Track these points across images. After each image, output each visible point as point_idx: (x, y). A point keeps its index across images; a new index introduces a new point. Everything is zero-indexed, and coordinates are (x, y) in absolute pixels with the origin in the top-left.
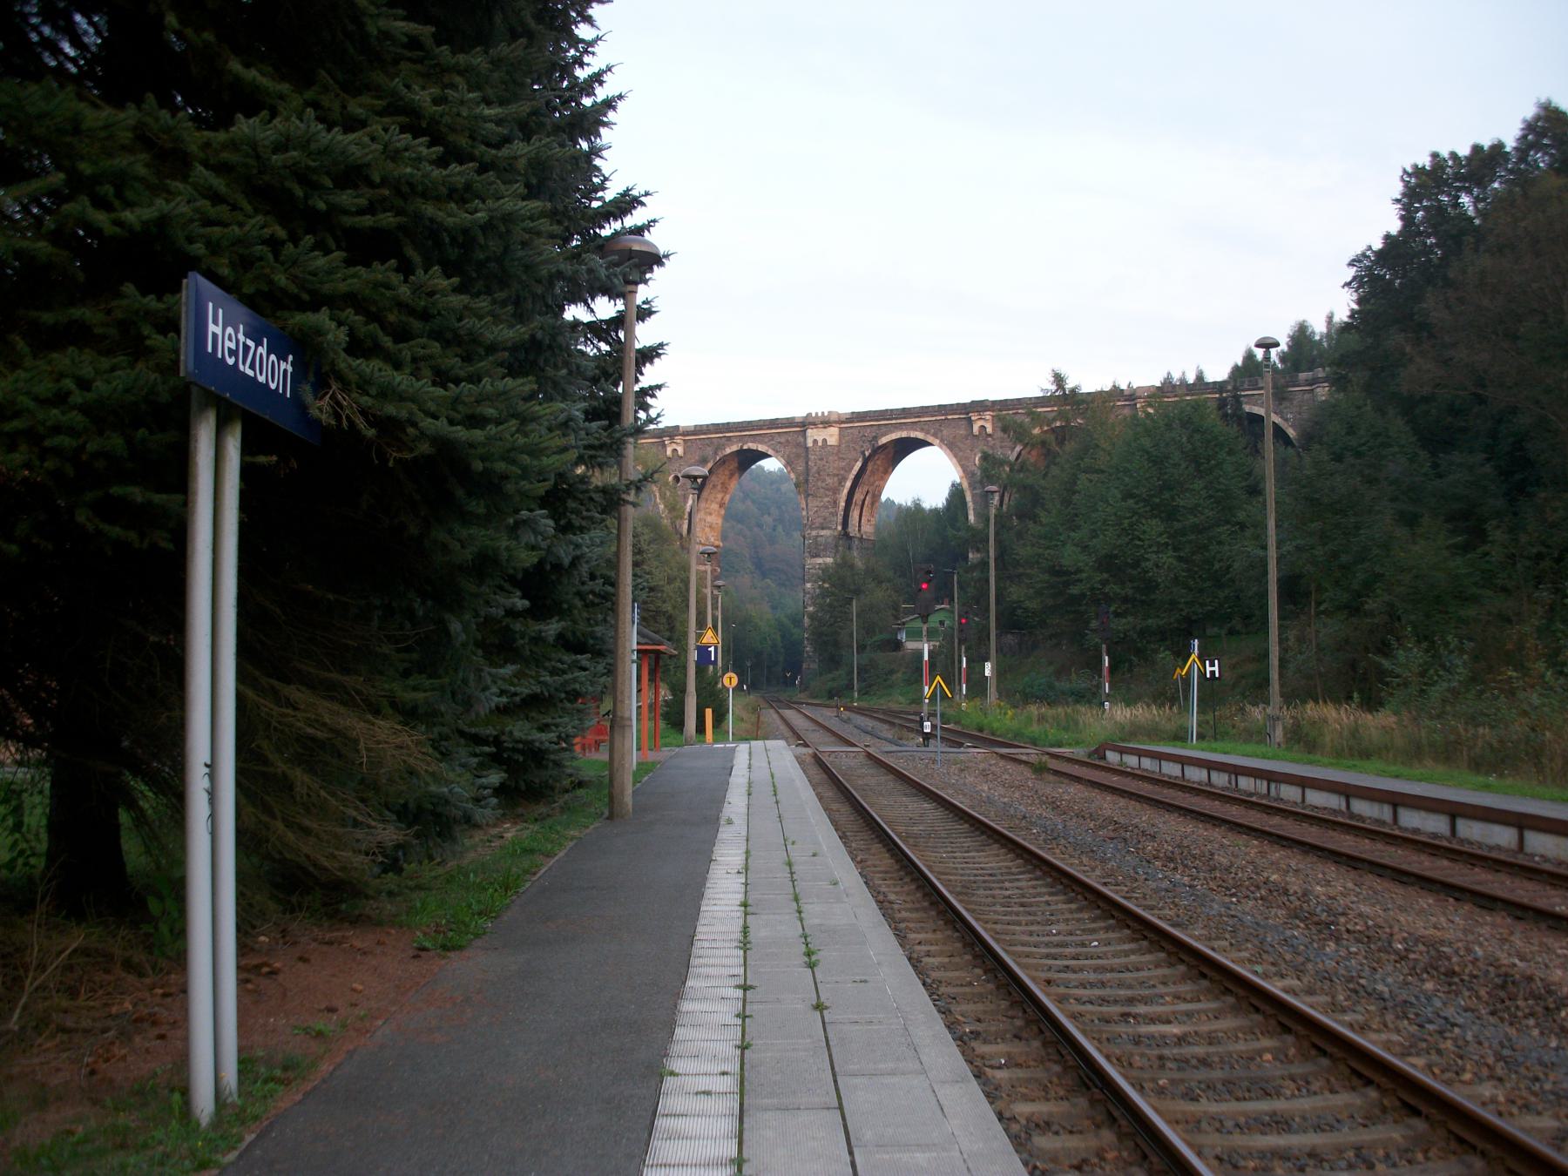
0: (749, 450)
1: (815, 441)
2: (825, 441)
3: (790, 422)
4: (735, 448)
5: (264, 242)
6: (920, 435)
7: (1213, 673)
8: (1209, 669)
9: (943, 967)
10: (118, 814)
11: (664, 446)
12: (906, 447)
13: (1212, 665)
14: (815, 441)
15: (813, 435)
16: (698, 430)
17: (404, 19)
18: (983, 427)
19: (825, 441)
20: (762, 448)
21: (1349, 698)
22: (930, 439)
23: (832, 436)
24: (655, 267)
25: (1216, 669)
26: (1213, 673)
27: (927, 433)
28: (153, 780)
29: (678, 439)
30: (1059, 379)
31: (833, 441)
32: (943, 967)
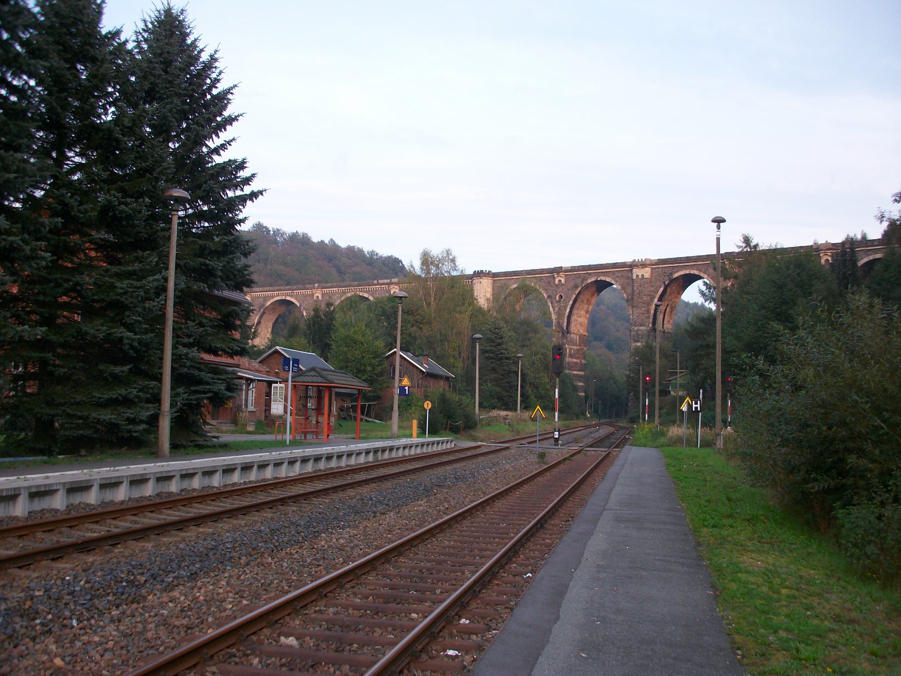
0: (601, 281)
1: (637, 276)
2: (643, 275)
3: (624, 265)
4: (593, 279)
6: (696, 272)
7: (696, 408)
8: (694, 406)
12: (690, 279)
13: (696, 403)
14: (637, 276)
15: (637, 272)
16: (573, 269)
20: (608, 279)
22: (702, 275)
25: (698, 406)
26: (696, 408)
27: (700, 271)
29: (562, 274)
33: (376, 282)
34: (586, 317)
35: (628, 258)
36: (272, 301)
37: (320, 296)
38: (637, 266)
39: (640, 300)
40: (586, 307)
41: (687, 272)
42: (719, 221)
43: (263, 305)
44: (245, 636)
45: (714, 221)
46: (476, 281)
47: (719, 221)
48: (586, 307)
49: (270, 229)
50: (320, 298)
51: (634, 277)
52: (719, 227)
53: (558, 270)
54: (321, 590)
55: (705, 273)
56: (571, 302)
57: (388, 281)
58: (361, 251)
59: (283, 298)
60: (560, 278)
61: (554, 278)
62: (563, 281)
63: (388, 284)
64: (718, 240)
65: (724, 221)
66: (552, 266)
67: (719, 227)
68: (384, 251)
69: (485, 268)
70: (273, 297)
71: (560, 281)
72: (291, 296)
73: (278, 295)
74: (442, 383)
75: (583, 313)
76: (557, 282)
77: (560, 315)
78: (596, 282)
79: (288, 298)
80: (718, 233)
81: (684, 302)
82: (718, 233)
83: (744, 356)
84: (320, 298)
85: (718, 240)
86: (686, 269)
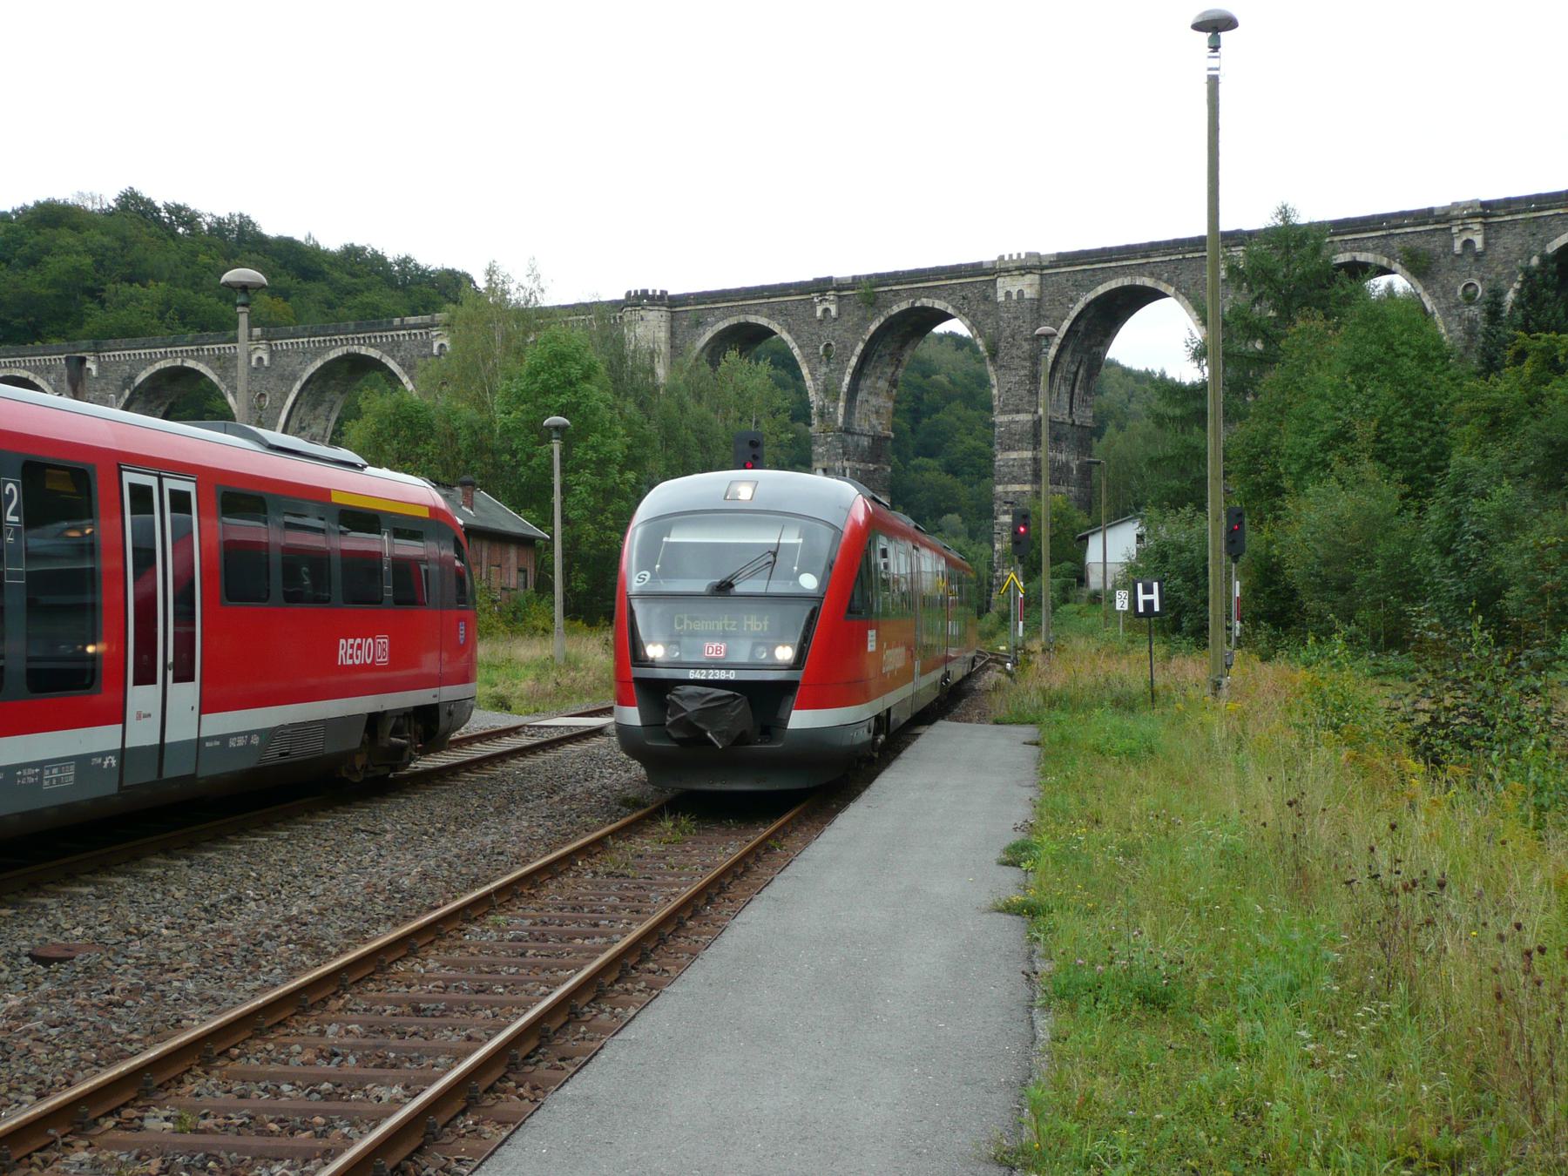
1: (1008, 294)
2: (1020, 292)
3: (976, 269)
4: (904, 306)
6: (1148, 282)
7: (1149, 604)
14: (1008, 294)
15: (1007, 286)
16: (856, 281)
19: (1020, 292)
22: (1162, 287)
25: (1155, 597)
26: (1149, 604)
27: (1159, 278)
29: (831, 295)
33: (397, 321)
34: (890, 397)
35: (986, 254)
36: (151, 370)
37: (266, 358)
38: (1008, 271)
39: (1014, 352)
40: (889, 371)
41: (1126, 281)
42: (1216, 26)
43: (132, 378)
44: (13, 1159)
45: (1198, 27)
46: (628, 315)
47: (1216, 26)
48: (889, 371)
49: (159, 204)
50: (266, 363)
51: (1001, 297)
52: (1215, 47)
53: (822, 286)
54: (382, 957)
55: (1169, 282)
56: (854, 361)
57: (427, 318)
58: (379, 259)
59: (179, 362)
60: (826, 305)
61: (814, 306)
62: (834, 311)
63: (426, 326)
64: (1213, 83)
65: (1228, 23)
66: (807, 276)
67: (1215, 47)
68: (432, 258)
69: (654, 285)
70: (152, 362)
71: (826, 310)
72: (198, 359)
73: (165, 357)
74: (513, 553)
75: (883, 384)
76: (819, 313)
77: (829, 390)
78: (912, 311)
79: (190, 364)
80: (1214, 63)
81: (1127, 372)
82: (1214, 63)
83: (514, 826)
84: (266, 363)
85: (1213, 83)
86: (1125, 275)
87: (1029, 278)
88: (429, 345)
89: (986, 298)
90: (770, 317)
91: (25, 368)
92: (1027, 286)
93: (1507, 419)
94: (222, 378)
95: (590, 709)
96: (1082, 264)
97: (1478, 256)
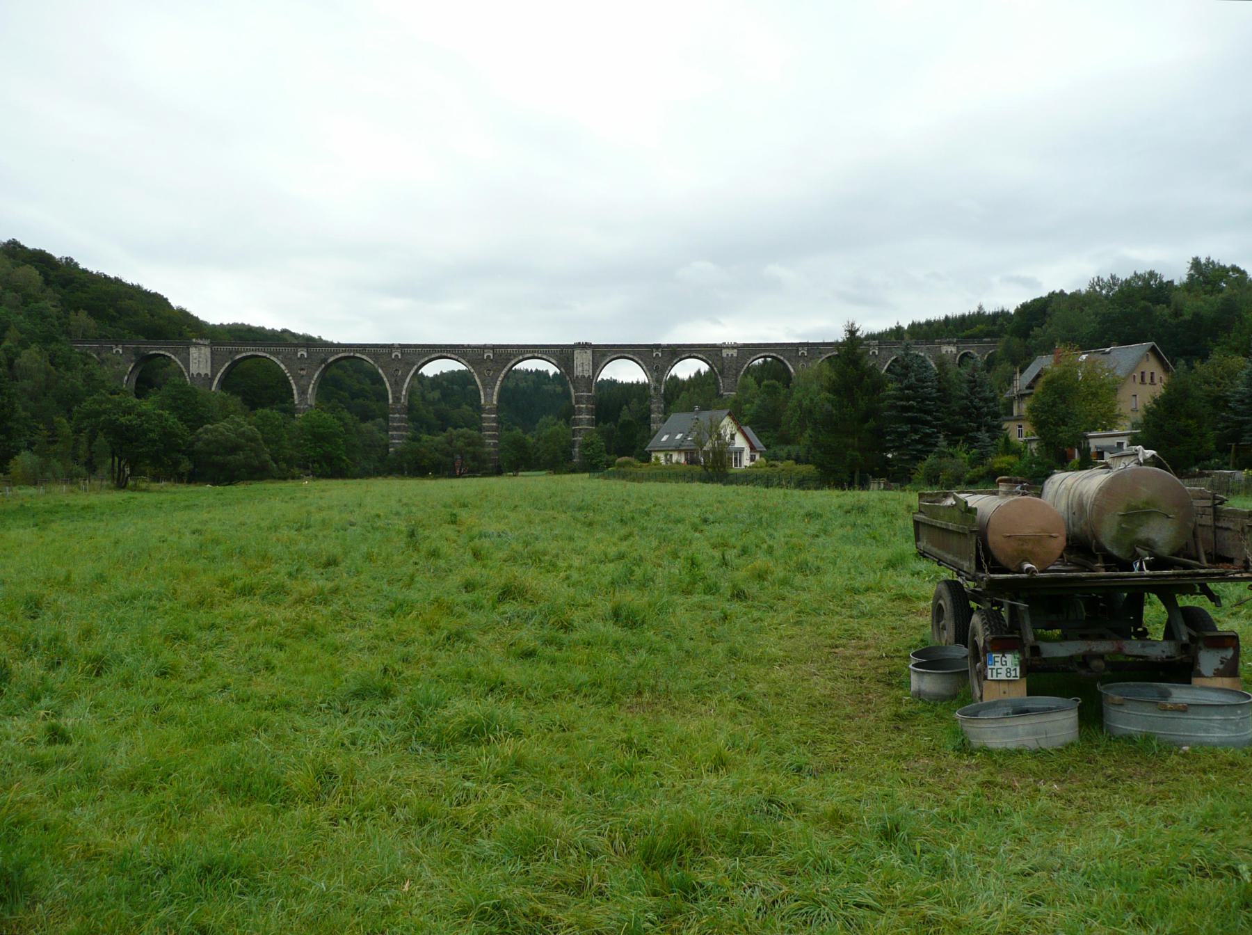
1: (947, 351)
2: (732, 355)
5: (1143, 299)
9: (401, 420)
10: (612, 383)
11: (869, 350)
14: (947, 351)
15: (725, 353)
16: (669, 346)
17: (1064, 638)
18: (803, 353)
19: (732, 355)
21: (91, 467)
23: (730, 352)
24: (1203, 261)
27: (778, 354)
28: (471, 384)
29: (660, 350)
30: (980, 308)
31: (735, 355)
32: (401, 420)
43: (326, 360)
53: (658, 346)
60: (396, 353)
67: (898, 323)
71: (657, 355)
87: (736, 350)
88: (391, 354)
89: (717, 355)
90: (634, 355)
91: (264, 352)
92: (735, 353)
93: (38, 699)
94: (375, 362)
95: (913, 535)
96: (157, 349)
97: (876, 356)
